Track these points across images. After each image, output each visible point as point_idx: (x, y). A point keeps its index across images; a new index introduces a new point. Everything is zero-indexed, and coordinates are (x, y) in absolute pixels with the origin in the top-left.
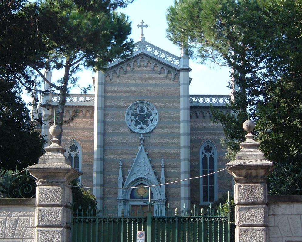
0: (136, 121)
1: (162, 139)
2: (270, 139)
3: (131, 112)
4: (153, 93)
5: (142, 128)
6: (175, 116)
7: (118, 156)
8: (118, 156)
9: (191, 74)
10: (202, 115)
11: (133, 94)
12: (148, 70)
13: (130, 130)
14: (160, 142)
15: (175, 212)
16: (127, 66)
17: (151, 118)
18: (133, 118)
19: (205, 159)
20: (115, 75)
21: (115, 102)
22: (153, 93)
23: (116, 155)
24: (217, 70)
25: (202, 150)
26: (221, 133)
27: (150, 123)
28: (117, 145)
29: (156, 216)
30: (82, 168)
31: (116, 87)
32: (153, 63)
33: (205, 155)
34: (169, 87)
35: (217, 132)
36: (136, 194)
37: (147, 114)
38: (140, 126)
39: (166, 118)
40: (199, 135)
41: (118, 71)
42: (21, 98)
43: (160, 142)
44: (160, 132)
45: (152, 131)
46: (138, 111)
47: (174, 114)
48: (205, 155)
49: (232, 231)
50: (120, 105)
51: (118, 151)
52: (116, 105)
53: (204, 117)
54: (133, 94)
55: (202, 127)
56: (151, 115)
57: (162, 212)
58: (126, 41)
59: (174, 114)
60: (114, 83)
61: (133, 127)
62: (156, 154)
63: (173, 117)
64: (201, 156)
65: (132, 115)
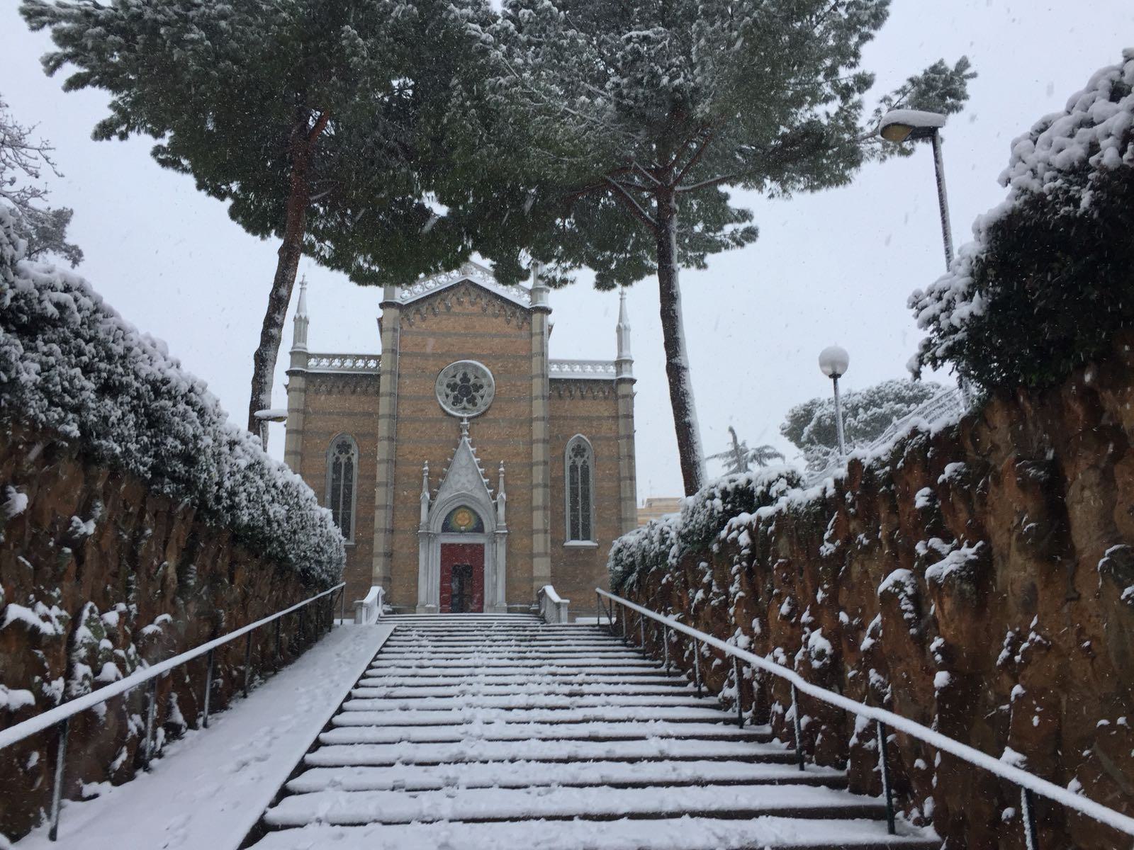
0: (455, 397)
2: (21, 447)
3: (446, 382)
9: (551, 319)
10: (578, 393)
12: (476, 309)
15: (1020, 650)
17: (481, 392)
18: (449, 391)
19: (573, 468)
20: (418, 317)
24: (888, 241)
25: (569, 452)
27: (478, 400)
33: (338, 459)
37: (475, 385)
38: (462, 405)
41: (423, 310)
42: (794, 194)
45: (484, 413)
46: (458, 380)
48: (574, 462)
53: (583, 397)
56: (481, 387)
58: (833, 93)
64: (568, 463)
65: (448, 386)
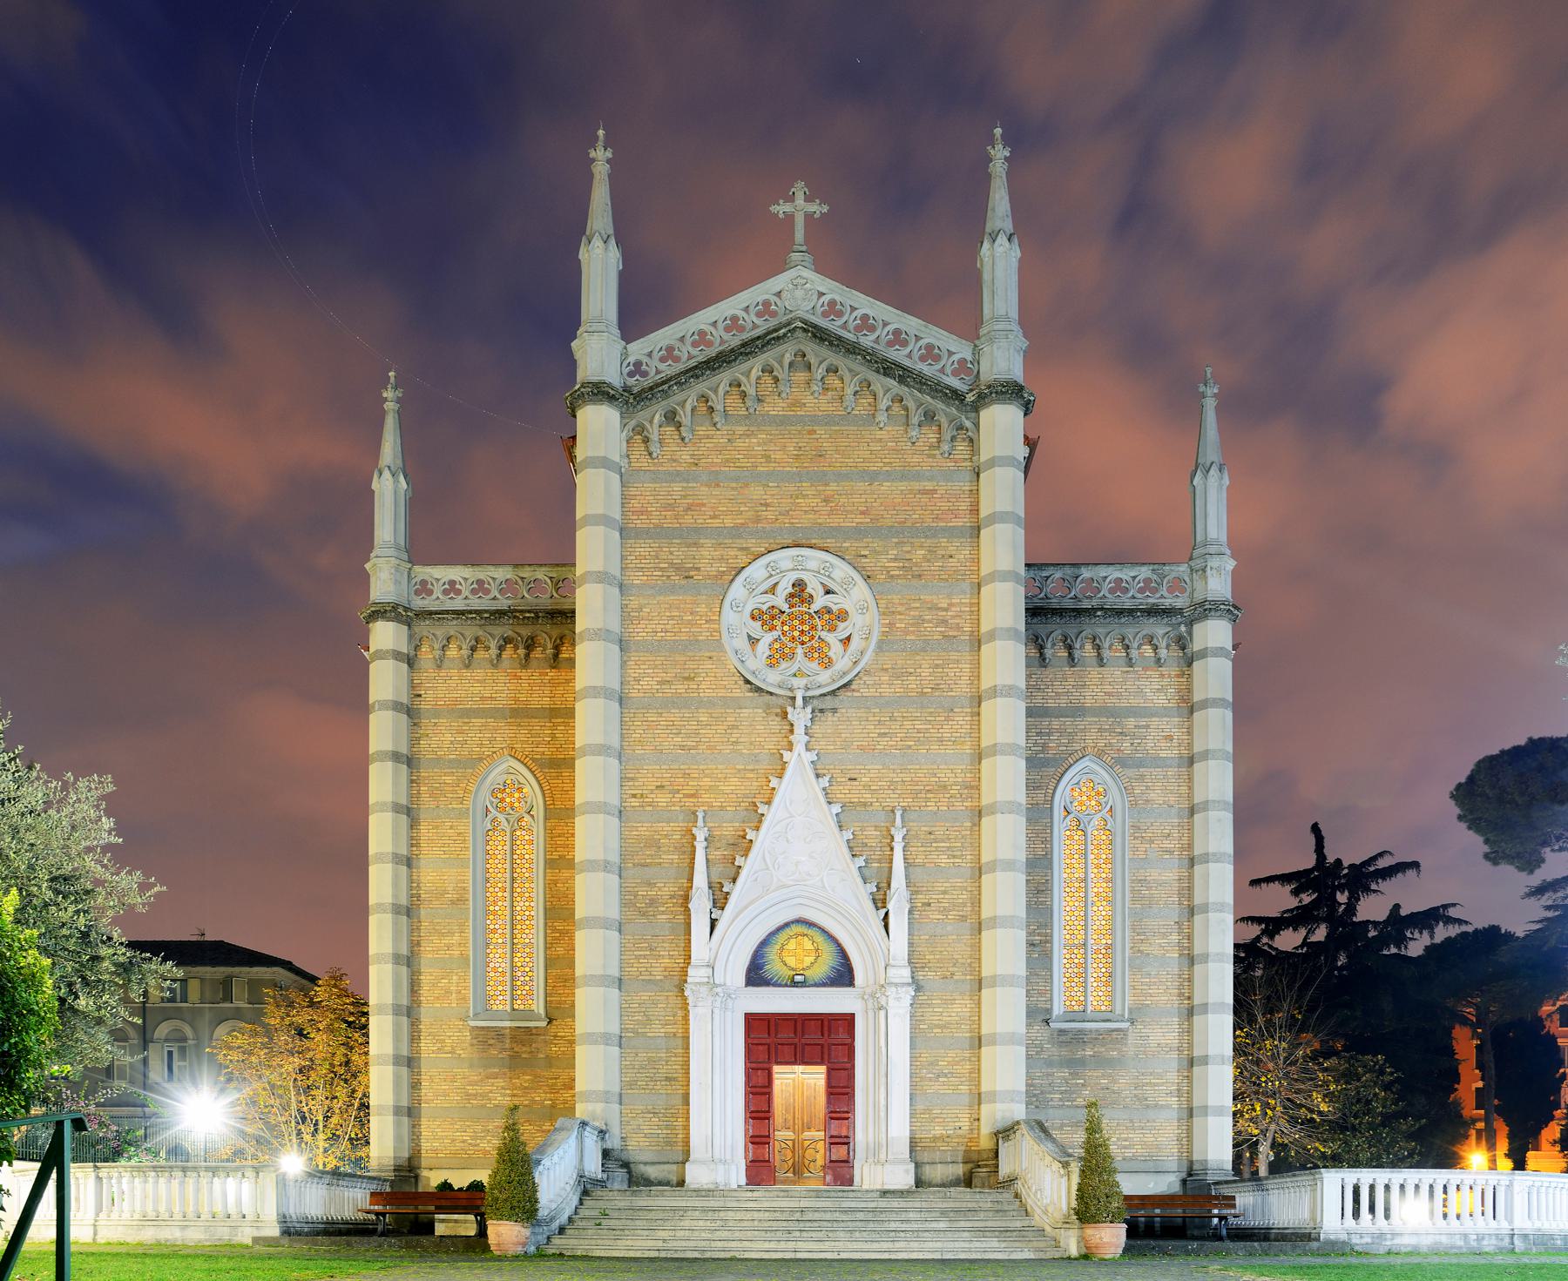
1: (892, 719)
4: (851, 512)
5: (773, 590)
6: (953, 617)
7: (692, 796)
8: (692, 796)
11: (758, 520)
13: (742, 683)
14: (881, 735)
16: (728, 388)
21: (671, 553)
22: (851, 512)
23: (678, 791)
26: (1147, 727)
28: (682, 748)
29: (821, 1073)
30: (545, 873)
31: (677, 487)
32: (854, 373)
34: (929, 486)
35: (1131, 722)
36: (774, 967)
39: (912, 625)
40: (1049, 734)
43: (881, 735)
44: (886, 691)
47: (951, 605)
49: (813, 1036)
50: (698, 569)
51: (686, 775)
52: (678, 568)
54: (758, 520)
55: (1063, 702)
57: (1433, 1192)
59: (951, 605)
60: (667, 467)
61: (755, 663)
62: (867, 787)
63: (944, 622)
